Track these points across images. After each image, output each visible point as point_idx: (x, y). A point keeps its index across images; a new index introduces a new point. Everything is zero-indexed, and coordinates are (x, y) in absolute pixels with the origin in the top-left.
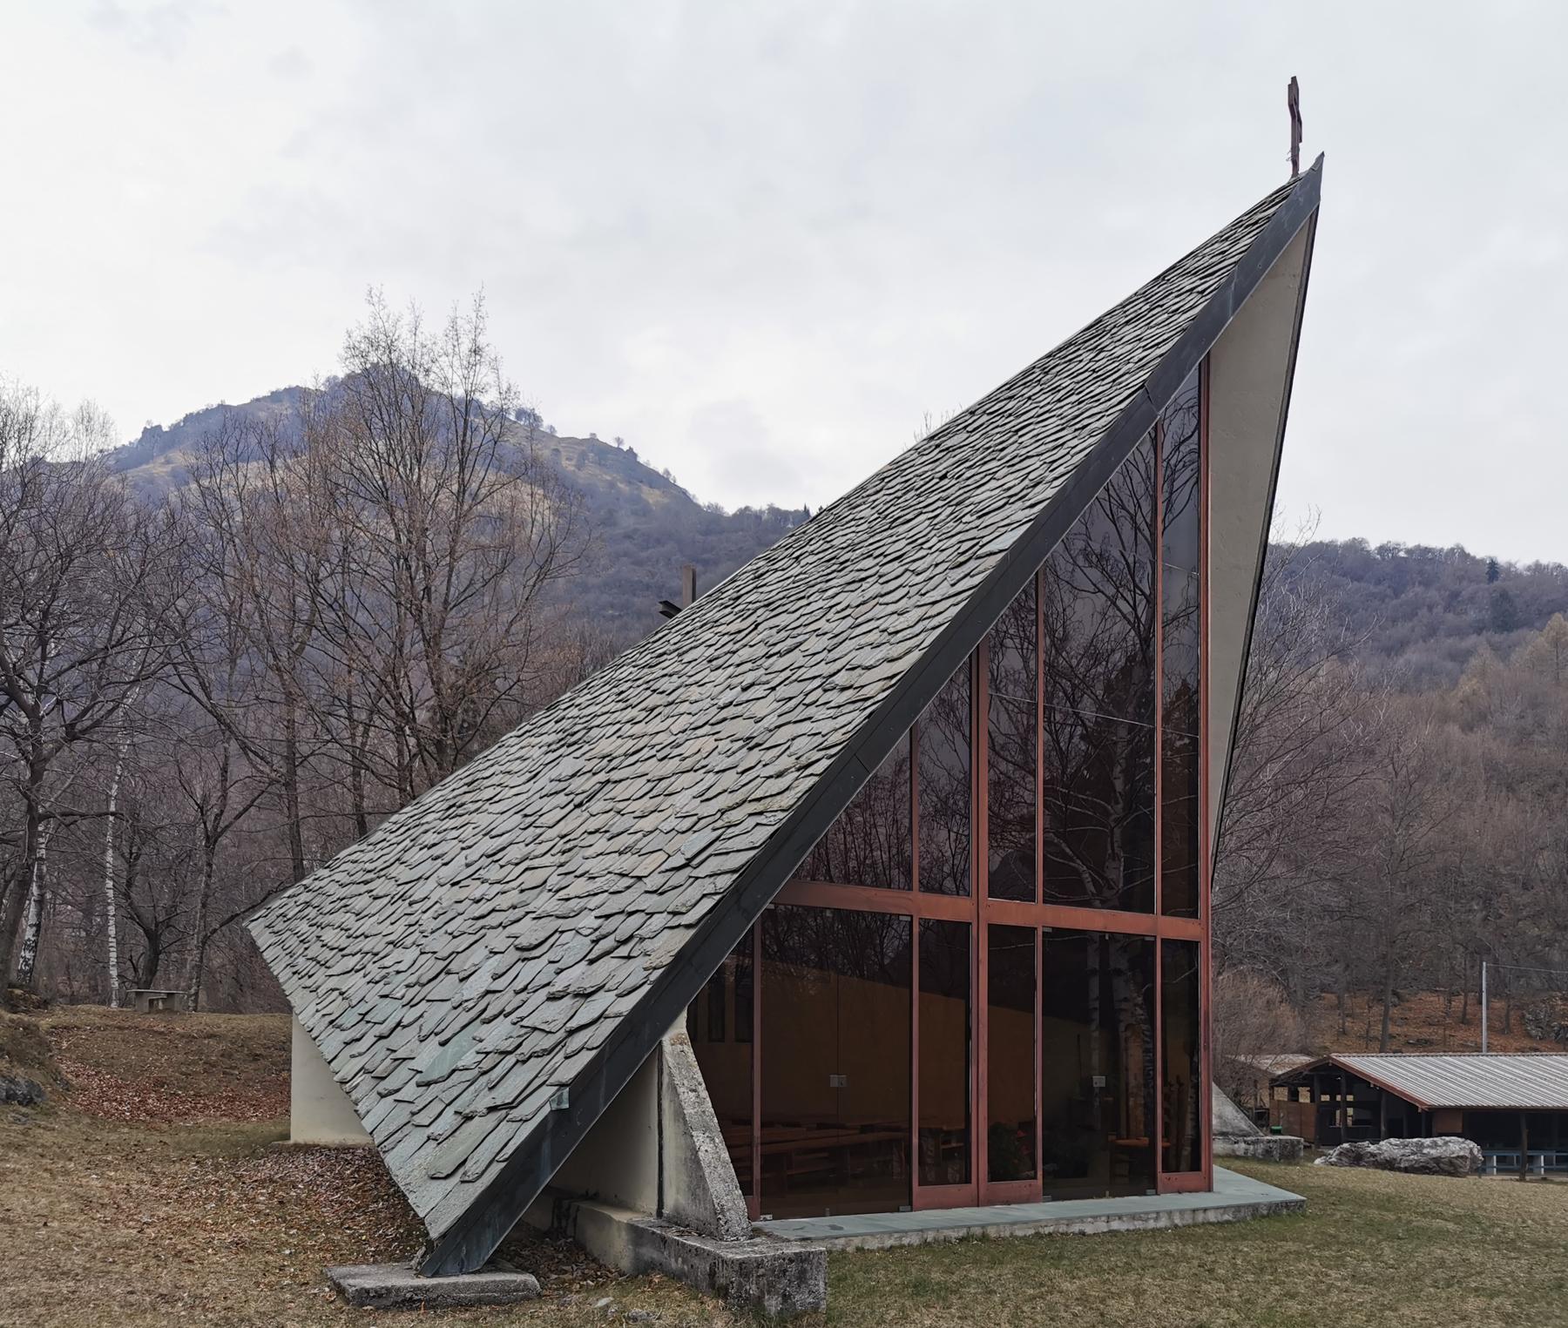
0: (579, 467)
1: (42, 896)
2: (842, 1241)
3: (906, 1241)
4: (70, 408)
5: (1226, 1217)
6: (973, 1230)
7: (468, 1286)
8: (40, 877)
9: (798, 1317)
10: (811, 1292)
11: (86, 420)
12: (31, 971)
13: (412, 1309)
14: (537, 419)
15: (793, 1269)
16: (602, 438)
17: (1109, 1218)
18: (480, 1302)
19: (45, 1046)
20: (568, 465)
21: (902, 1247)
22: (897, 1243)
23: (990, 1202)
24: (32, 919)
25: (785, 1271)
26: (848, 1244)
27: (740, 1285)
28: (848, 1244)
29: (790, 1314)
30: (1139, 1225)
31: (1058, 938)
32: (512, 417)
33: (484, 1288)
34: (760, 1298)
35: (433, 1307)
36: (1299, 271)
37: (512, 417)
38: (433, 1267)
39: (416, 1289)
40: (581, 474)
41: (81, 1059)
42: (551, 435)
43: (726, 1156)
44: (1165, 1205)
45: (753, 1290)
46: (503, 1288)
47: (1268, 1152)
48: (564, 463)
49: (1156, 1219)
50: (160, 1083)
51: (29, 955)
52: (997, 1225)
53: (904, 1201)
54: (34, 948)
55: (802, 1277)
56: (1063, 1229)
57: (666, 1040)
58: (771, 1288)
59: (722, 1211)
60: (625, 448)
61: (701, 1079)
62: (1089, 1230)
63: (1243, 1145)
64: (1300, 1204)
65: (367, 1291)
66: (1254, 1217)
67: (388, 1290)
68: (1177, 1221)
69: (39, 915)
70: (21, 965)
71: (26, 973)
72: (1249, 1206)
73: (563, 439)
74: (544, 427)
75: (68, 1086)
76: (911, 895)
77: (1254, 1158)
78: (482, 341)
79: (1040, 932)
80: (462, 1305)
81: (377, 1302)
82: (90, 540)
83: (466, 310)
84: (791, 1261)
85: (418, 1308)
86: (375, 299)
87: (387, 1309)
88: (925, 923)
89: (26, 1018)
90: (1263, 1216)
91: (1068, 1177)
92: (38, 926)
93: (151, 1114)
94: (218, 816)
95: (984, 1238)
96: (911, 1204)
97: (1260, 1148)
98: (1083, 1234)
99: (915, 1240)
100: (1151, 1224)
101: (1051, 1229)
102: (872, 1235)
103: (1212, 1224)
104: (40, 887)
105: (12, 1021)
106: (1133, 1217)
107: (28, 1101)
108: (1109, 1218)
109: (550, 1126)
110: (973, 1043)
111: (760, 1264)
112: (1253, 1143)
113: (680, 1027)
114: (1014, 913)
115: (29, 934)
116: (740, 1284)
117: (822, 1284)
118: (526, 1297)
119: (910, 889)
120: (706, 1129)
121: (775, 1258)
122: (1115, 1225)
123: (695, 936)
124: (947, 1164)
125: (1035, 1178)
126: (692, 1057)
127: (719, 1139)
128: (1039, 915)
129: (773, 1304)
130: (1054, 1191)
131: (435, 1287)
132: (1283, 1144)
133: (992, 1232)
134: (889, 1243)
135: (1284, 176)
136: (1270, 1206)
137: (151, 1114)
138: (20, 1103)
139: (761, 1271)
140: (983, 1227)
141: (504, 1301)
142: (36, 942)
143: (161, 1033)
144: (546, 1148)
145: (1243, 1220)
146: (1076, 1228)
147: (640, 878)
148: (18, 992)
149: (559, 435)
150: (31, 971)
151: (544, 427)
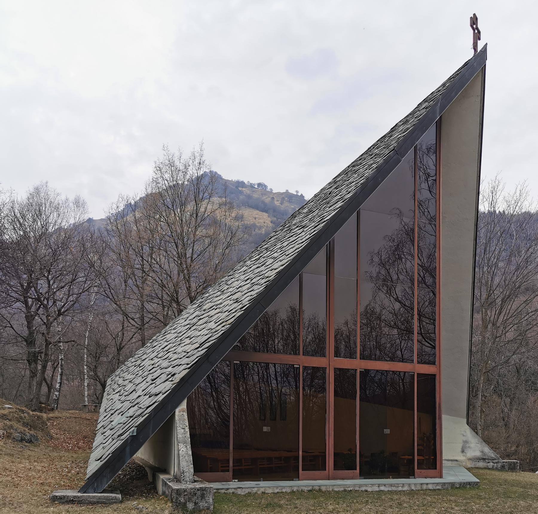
0: (282, 203)
1: (62, 372)
2: (256, 489)
3: (284, 490)
4: (72, 198)
5: (438, 487)
6: (314, 488)
7: (94, 497)
8: (61, 366)
9: (200, 511)
10: (206, 502)
11: (79, 203)
12: (58, 399)
13: (73, 504)
14: (266, 186)
15: (199, 493)
16: (290, 191)
17: (379, 485)
18: (98, 503)
19: (44, 423)
20: (277, 203)
21: (282, 492)
22: (280, 491)
23: (334, 478)
24: (59, 381)
25: (195, 494)
26: (258, 490)
27: (177, 498)
28: (258, 490)
29: (197, 509)
30: (394, 489)
31: (365, 373)
32: (256, 187)
33: (100, 498)
34: (185, 504)
35: (80, 503)
36: (479, 94)
37: (256, 187)
38: (84, 490)
39: (75, 497)
40: (283, 206)
41: (60, 429)
42: (271, 192)
43: (190, 453)
44: (419, 482)
45: (182, 500)
46: (107, 498)
47: (503, 467)
48: (276, 203)
49: (403, 487)
50: (85, 437)
51: (57, 393)
52: (326, 486)
53: (296, 477)
54: (59, 391)
55: (203, 497)
56: (357, 489)
57: (177, 410)
58: (190, 500)
59: (183, 473)
60: (299, 194)
61: (188, 425)
62: (370, 489)
63: (492, 464)
64: (477, 483)
65: (57, 497)
66: (452, 488)
67: (64, 497)
68: (413, 488)
69: (61, 379)
70: (55, 397)
71: (56, 400)
72: (449, 483)
73: (275, 193)
74: (268, 190)
75: (52, 438)
76: (299, 357)
77: (497, 469)
78: (203, 159)
79: (358, 371)
80: (93, 503)
81: (60, 500)
82: (65, 245)
83: (197, 149)
84: (198, 490)
85: (75, 503)
86: (166, 148)
87: (63, 503)
88: (305, 368)
89: (38, 414)
90: (457, 488)
91: (370, 471)
92: (61, 383)
93: (79, 448)
94: (121, 344)
95: (320, 490)
96: (299, 478)
97: (499, 465)
98: (366, 491)
99: (289, 490)
100: (400, 489)
101: (351, 489)
102: (269, 487)
103: (430, 490)
104: (61, 369)
105: (33, 414)
106: (391, 485)
107: (30, 441)
108: (379, 485)
109: (129, 441)
110: (327, 415)
111: (185, 491)
112: (496, 463)
113: (184, 405)
114: (345, 363)
115: (58, 386)
116: (177, 498)
117: (211, 499)
118: (115, 501)
119: (299, 355)
120: (185, 442)
121: (191, 489)
122: (382, 488)
123: (189, 372)
124: (315, 463)
125: (356, 469)
126: (186, 417)
127: (189, 447)
128: (357, 364)
129: (190, 506)
130: (364, 474)
131: (81, 496)
132: (510, 464)
133: (323, 489)
134: (276, 491)
135: (470, 54)
136: (460, 484)
137: (79, 448)
138: (26, 442)
139: (186, 493)
140: (319, 486)
141: (106, 503)
142: (60, 389)
143: (89, 419)
144: (128, 449)
145: (447, 489)
146: (363, 489)
147: (188, 352)
148: (43, 405)
149: (274, 192)
150: (58, 399)
151: (268, 190)
